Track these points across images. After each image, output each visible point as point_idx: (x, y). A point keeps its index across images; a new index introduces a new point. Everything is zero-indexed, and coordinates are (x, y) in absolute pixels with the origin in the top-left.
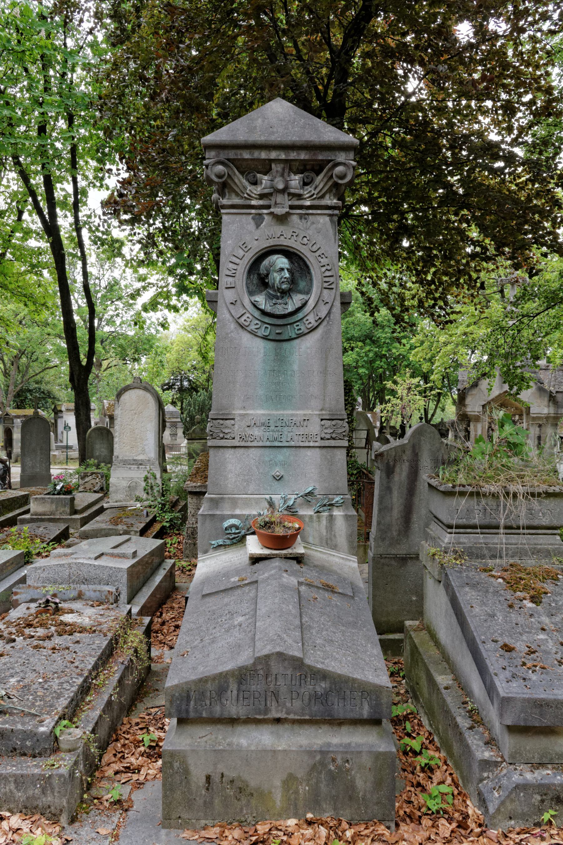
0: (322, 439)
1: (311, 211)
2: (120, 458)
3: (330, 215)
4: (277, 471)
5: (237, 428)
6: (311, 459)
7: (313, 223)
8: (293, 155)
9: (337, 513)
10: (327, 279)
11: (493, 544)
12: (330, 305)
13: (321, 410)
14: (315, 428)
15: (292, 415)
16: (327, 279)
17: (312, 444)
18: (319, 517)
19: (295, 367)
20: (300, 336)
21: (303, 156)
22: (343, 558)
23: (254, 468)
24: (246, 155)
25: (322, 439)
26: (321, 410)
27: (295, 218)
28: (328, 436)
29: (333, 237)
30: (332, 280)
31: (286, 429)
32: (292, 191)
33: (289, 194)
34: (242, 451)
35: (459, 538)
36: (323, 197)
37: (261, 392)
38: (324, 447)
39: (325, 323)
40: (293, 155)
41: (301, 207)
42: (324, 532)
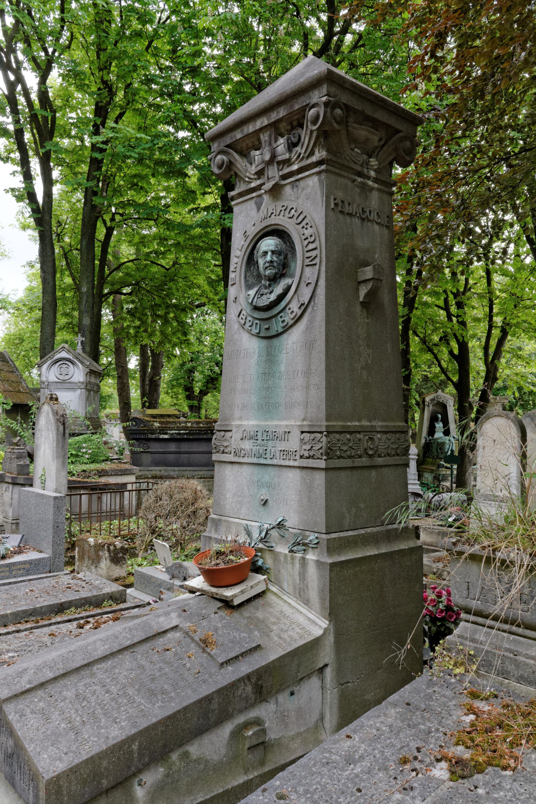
0: (301, 457)
1: (300, 176)
2: (482, 491)
4: (264, 494)
5: (234, 440)
6: (292, 480)
7: (303, 189)
8: (274, 116)
9: (311, 556)
10: (309, 254)
11: (527, 656)
12: (313, 285)
13: (304, 420)
14: (294, 443)
15: (277, 426)
16: (309, 254)
17: (292, 463)
18: (293, 558)
19: (283, 368)
20: (287, 329)
21: (282, 112)
22: (310, 619)
23: (246, 488)
24: (238, 135)
25: (301, 457)
26: (304, 420)
27: (288, 190)
28: (306, 454)
31: (270, 443)
32: (280, 158)
33: (279, 163)
34: (237, 467)
35: (475, 632)
36: (312, 153)
37: (254, 399)
38: (303, 468)
40: (274, 116)
41: (291, 174)
42: (297, 578)
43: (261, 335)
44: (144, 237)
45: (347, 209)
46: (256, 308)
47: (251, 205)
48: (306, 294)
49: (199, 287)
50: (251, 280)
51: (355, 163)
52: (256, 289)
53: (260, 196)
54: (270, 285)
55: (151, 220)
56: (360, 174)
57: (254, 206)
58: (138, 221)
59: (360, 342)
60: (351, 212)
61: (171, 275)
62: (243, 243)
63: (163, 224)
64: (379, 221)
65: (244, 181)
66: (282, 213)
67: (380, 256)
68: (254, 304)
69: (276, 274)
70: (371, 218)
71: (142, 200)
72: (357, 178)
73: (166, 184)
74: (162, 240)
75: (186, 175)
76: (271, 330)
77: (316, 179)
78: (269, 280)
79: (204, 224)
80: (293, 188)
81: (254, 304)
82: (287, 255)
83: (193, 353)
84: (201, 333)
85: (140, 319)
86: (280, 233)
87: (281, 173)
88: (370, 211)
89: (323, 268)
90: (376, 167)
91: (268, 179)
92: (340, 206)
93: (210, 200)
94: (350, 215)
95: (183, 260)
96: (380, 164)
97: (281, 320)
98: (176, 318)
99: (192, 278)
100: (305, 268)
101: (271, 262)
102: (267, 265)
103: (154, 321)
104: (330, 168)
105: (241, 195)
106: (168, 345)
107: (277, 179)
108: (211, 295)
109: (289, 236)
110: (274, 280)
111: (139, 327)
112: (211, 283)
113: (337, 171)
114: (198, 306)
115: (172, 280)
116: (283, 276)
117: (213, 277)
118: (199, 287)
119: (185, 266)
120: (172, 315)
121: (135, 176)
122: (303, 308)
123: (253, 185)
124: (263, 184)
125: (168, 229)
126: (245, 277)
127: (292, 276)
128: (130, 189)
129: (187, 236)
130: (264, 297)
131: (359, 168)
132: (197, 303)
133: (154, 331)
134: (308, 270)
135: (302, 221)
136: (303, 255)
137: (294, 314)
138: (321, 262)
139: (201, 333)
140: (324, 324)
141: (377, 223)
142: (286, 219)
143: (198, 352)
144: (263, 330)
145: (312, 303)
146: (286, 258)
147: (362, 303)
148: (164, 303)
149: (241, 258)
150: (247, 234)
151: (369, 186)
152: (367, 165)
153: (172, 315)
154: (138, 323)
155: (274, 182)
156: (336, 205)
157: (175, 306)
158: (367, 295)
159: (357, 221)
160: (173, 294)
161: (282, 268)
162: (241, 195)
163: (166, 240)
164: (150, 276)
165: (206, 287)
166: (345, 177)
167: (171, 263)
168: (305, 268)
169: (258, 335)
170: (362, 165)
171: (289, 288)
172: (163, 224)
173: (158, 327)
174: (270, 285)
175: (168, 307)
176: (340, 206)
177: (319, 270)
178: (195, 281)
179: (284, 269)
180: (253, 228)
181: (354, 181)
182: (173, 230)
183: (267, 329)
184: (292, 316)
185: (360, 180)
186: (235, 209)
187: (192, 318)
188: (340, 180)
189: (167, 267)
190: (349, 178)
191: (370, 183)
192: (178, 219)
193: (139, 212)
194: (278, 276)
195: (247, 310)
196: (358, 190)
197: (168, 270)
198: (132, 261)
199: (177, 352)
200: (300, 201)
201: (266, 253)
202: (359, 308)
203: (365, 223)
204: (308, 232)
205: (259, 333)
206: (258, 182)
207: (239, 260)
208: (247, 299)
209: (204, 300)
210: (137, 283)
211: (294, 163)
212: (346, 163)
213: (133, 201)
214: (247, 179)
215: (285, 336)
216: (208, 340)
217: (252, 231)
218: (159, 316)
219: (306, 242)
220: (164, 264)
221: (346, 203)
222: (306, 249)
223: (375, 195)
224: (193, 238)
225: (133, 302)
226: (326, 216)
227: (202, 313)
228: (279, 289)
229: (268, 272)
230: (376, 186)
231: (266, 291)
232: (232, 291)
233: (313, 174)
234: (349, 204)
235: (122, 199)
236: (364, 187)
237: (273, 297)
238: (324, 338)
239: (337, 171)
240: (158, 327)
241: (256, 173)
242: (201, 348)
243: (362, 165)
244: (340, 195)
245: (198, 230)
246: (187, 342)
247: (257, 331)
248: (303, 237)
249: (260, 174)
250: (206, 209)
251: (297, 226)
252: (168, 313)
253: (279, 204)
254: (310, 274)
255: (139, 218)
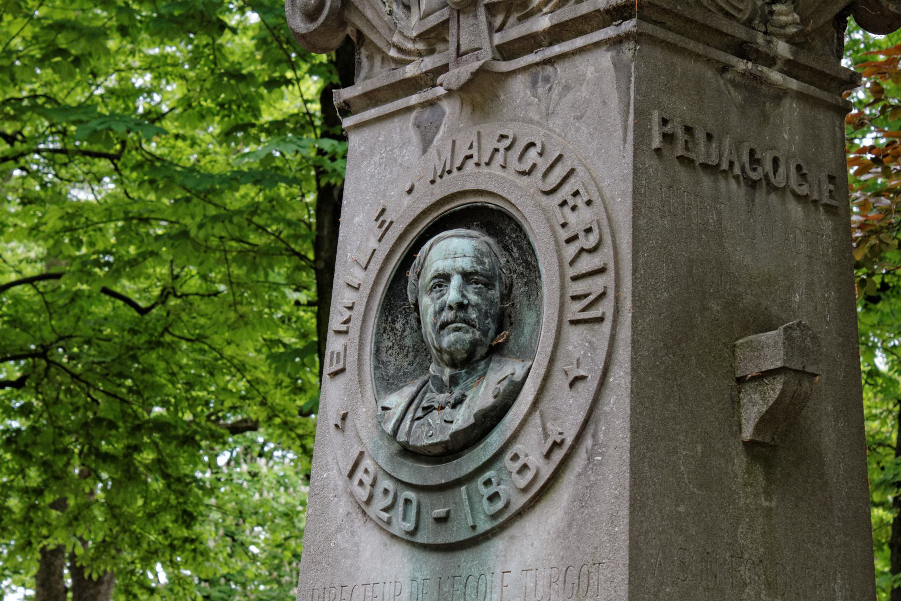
1: (557, 49)
3: (617, 42)
7: (567, 88)
10: (579, 288)
16: (579, 288)
20: (505, 522)
27: (519, 86)
29: (619, 122)
30: (595, 285)
39: (579, 463)
41: (531, 42)
43: (421, 538)
44: (81, 208)
45: (701, 153)
46: (408, 452)
47: (404, 131)
48: (567, 411)
49: (242, 369)
50: (394, 362)
51: (727, 14)
52: (409, 391)
53: (431, 104)
54: (454, 381)
55: (99, 155)
56: (743, 50)
57: (413, 136)
58: (62, 158)
59: (745, 572)
60: (713, 160)
61: (152, 330)
62: (373, 244)
63: (138, 166)
64: (804, 190)
65: (385, 58)
66: (499, 158)
67: (806, 297)
68: (402, 437)
69: (474, 344)
70: (779, 180)
71: (79, 97)
72: (733, 60)
73: (156, 51)
74: (135, 220)
75: (222, 26)
76: (453, 525)
77: (605, 58)
78: (453, 364)
79: (268, 174)
80: (534, 83)
81: (402, 437)
82: (511, 287)
83: (212, 582)
84: (241, 514)
85: (45, 465)
86: (486, 217)
87: (498, 39)
88: (776, 161)
89: (625, 333)
90: (792, 30)
91: (459, 55)
92: (680, 144)
93: (286, 104)
94: (711, 169)
95: (194, 284)
96: (804, 21)
97: (487, 492)
98: (161, 466)
99: (218, 340)
100: (567, 327)
101: (461, 306)
102: (448, 315)
103: (89, 473)
104: (648, 28)
105: (372, 98)
106: (127, 555)
107: (486, 55)
108: (278, 397)
109: (519, 228)
110: (468, 363)
111: (38, 492)
112: (282, 359)
113: (671, 37)
114: (235, 429)
115: (154, 344)
116: (496, 351)
117: (290, 338)
118: (242, 369)
119: (202, 305)
120: (148, 456)
121: (60, 26)
122: (558, 456)
123: (411, 71)
124: (445, 68)
125: (152, 182)
126: (378, 350)
127: (526, 354)
128: (42, 62)
129: (212, 211)
130: (435, 418)
131: (741, 33)
132: (231, 419)
133: (88, 506)
134: (575, 337)
135: (559, 184)
136: (563, 287)
137: (529, 475)
138: (617, 311)
139: (241, 514)
140: (625, 511)
141: (798, 197)
142: (510, 175)
143: (228, 578)
144: (427, 522)
145: (588, 442)
146: (507, 295)
147: (749, 445)
148: (124, 414)
149: (366, 291)
150: (388, 217)
151: (771, 84)
152: (765, 22)
153: (148, 456)
154: (34, 476)
155: (476, 65)
156: (668, 138)
157: (160, 426)
158: (764, 422)
159: (733, 189)
160: (157, 388)
161: (494, 328)
162: (372, 98)
163: (146, 221)
164: (86, 330)
165: (264, 372)
166: (698, 56)
167: (156, 292)
168: (567, 327)
169: (410, 540)
170: (749, 23)
171: (515, 390)
172: (138, 166)
173: (100, 495)
174: (454, 381)
175: (137, 428)
176: (680, 144)
177: (613, 338)
178: (229, 351)
179: (499, 331)
180: (407, 200)
181: (725, 68)
182: (167, 190)
183: (442, 520)
184: (522, 482)
185: (742, 65)
186: (355, 141)
187: (212, 465)
188: (682, 64)
189: (143, 304)
190: (709, 61)
191: (776, 76)
192: (189, 157)
193: (64, 133)
194: (481, 351)
195: (378, 456)
196: (737, 96)
197: (143, 311)
198: (30, 281)
199: (160, 575)
200: (556, 123)
201: (443, 279)
202: (740, 461)
203: (760, 195)
204: (577, 220)
205: (413, 533)
206: (429, 63)
207: (359, 299)
208: (380, 422)
209: (254, 411)
210: (44, 352)
211: (539, 10)
212: (699, 16)
213: (49, 98)
214: (393, 53)
215: (498, 544)
216: (259, 540)
217: (404, 210)
218: (106, 458)
219: (571, 250)
220: (135, 297)
221: (700, 136)
222: (571, 272)
223: (791, 110)
224: (225, 217)
225: (25, 411)
226: (636, 171)
227: (247, 450)
228: (482, 395)
229: (448, 339)
230: (794, 84)
231: (442, 398)
232: (334, 396)
233: (597, 45)
234: (709, 137)
235: (13, 93)
236: (753, 85)
237: (462, 418)
238: (623, 556)
239: (671, 37)
240: (100, 495)
241: (421, 37)
242: (237, 564)
243: (749, 23)
244: (682, 109)
245: (248, 193)
246: (195, 549)
247: (409, 526)
248: (564, 235)
249: (434, 37)
250: (277, 128)
251: (544, 200)
252: (137, 449)
253: (491, 131)
254: (583, 348)
255: (63, 151)
